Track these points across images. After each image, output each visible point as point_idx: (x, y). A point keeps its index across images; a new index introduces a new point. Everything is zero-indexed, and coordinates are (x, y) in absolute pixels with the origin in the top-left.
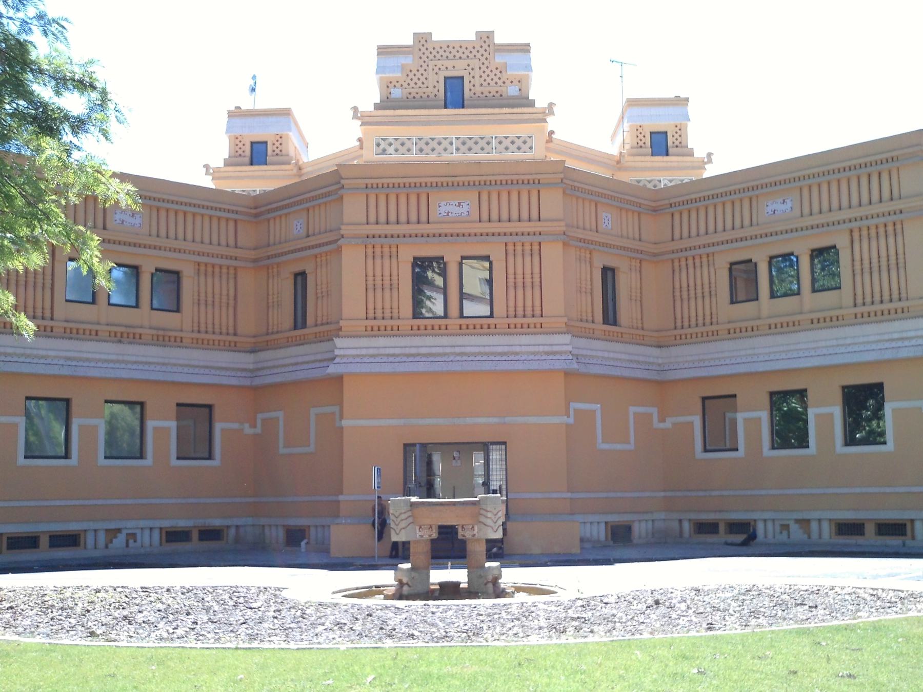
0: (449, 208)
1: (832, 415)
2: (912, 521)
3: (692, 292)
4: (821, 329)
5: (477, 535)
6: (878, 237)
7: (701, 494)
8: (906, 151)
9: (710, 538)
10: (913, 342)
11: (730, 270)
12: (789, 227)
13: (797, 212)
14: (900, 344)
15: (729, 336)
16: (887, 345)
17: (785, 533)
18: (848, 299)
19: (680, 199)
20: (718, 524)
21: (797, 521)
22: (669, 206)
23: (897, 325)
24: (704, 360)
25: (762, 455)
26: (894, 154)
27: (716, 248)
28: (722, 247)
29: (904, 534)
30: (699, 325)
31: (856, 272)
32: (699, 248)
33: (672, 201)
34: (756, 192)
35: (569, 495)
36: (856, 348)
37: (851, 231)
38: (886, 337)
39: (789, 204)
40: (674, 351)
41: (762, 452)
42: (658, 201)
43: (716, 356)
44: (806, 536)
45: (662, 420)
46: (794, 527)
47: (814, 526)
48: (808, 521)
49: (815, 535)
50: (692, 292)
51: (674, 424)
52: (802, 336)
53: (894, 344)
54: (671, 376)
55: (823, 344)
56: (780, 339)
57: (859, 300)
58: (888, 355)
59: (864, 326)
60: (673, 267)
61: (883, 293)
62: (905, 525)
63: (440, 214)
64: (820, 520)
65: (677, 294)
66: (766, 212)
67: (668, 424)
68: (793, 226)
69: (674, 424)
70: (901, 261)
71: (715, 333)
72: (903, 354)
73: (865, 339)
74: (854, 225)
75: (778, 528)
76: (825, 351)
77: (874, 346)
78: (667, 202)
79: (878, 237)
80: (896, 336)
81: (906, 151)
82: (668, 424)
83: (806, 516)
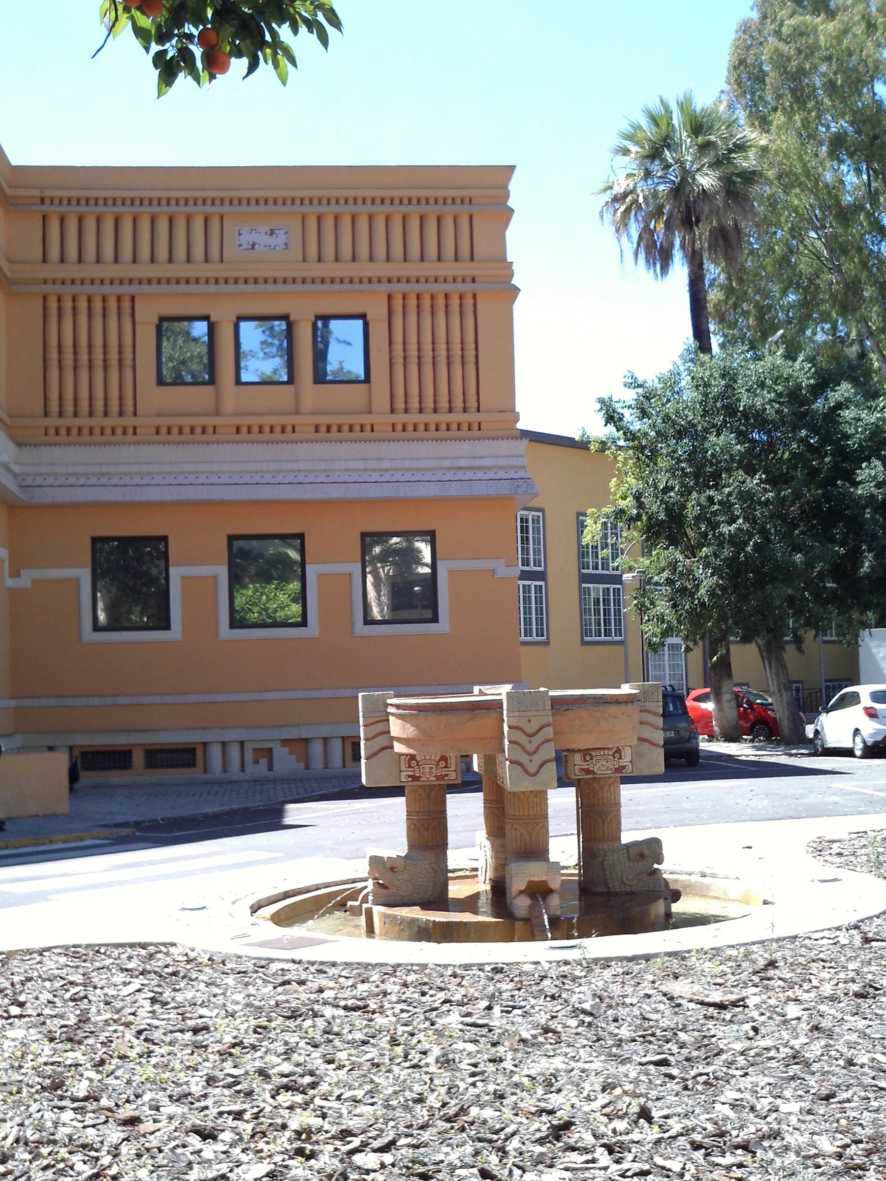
0: (254, 237)
1: (215, 578)
2: (205, 744)
3: (84, 357)
4: (253, 443)
5: (629, 769)
6: (104, 316)
7: (96, 701)
8: (487, 192)
9: (116, 777)
10: (491, 475)
11: (159, 327)
12: (280, 274)
13: (296, 252)
14: (470, 475)
15: (159, 438)
16: (449, 475)
17: (264, 762)
18: (381, 401)
19: (65, 193)
20: (130, 752)
21: (285, 742)
22: (39, 202)
23: (467, 447)
24: (108, 474)
25: (80, 638)
26: (467, 193)
27: (145, 288)
28: (154, 288)
29: (192, 764)
30: (424, 410)
31: (394, 360)
32: (436, 281)
33: (49, 193)
34: (226, 209)
35: (13, 703)
36: (398, 476)
37: (390, 297)
38: (448, 463)
39: (281, 238)
40: (46, 453)
41: (217, 631)
42: (17, 187)
43: (134, 469)
44: (302, 765)
45: (15, 574)
46: (280, 752)
47: (317, 748)
48: (307, 740)
49: (317, 763)
50: (84, 357)
51: (35, 581)
52: (302, 450)
53: (460, 475)
54: (46, 496)
55: (342, 465)
56: (261, 451)
57: (400, 405)
58: (455, 490)
59: (415, 444)
60: (45, 308)
61: (438, 398)
62: (194, 750)
63: (240, 246)
64: (325, 740)
65: (54, 355)
66: (237, 243)
67: (25, 580)
68: (289, 274)
69: (35, 581)
70: (128, 355)
71: (476, 426)
72: (480, 490)
73: (415, 464)
74: (394, 287)
75: (249, 755)
76: (345, 477)
77: (428, 476)
78: (37, 193)
79: (104, 316)
80: (463, 463)
81: (487, 192)
82: (25, 580)
83: (304, 733)
